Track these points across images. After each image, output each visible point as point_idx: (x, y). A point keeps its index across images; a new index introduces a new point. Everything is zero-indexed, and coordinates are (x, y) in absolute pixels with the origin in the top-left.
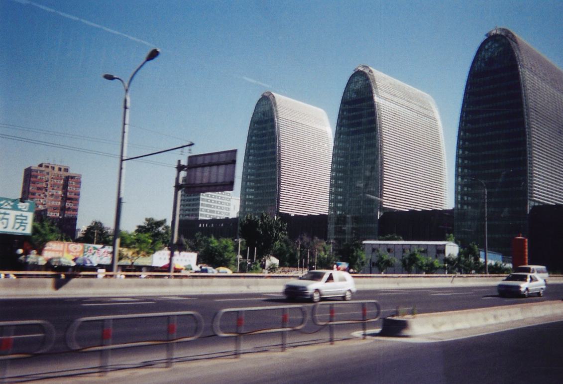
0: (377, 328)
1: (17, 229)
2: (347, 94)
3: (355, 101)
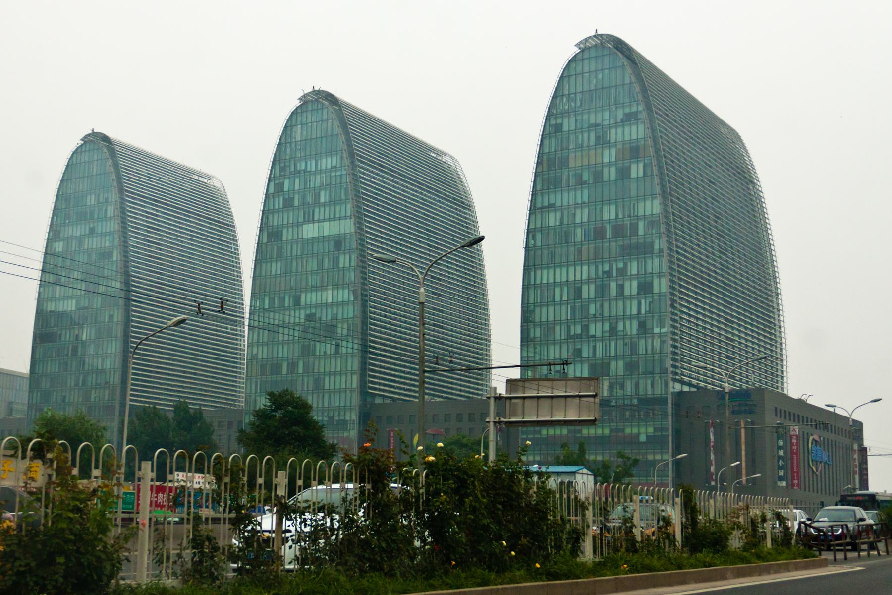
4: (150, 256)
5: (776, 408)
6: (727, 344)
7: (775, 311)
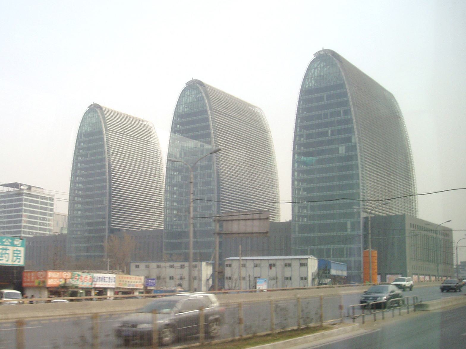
0: (297, 201)
1: (15, 261)
2: (180, 107)
3: (188, 115)
4: (119, 146)
5: (411, 224)
6: (389, 194)
7: (412, 177)
